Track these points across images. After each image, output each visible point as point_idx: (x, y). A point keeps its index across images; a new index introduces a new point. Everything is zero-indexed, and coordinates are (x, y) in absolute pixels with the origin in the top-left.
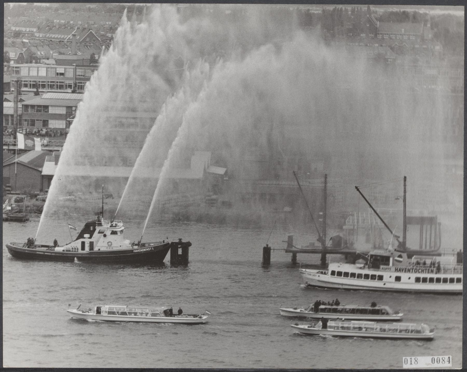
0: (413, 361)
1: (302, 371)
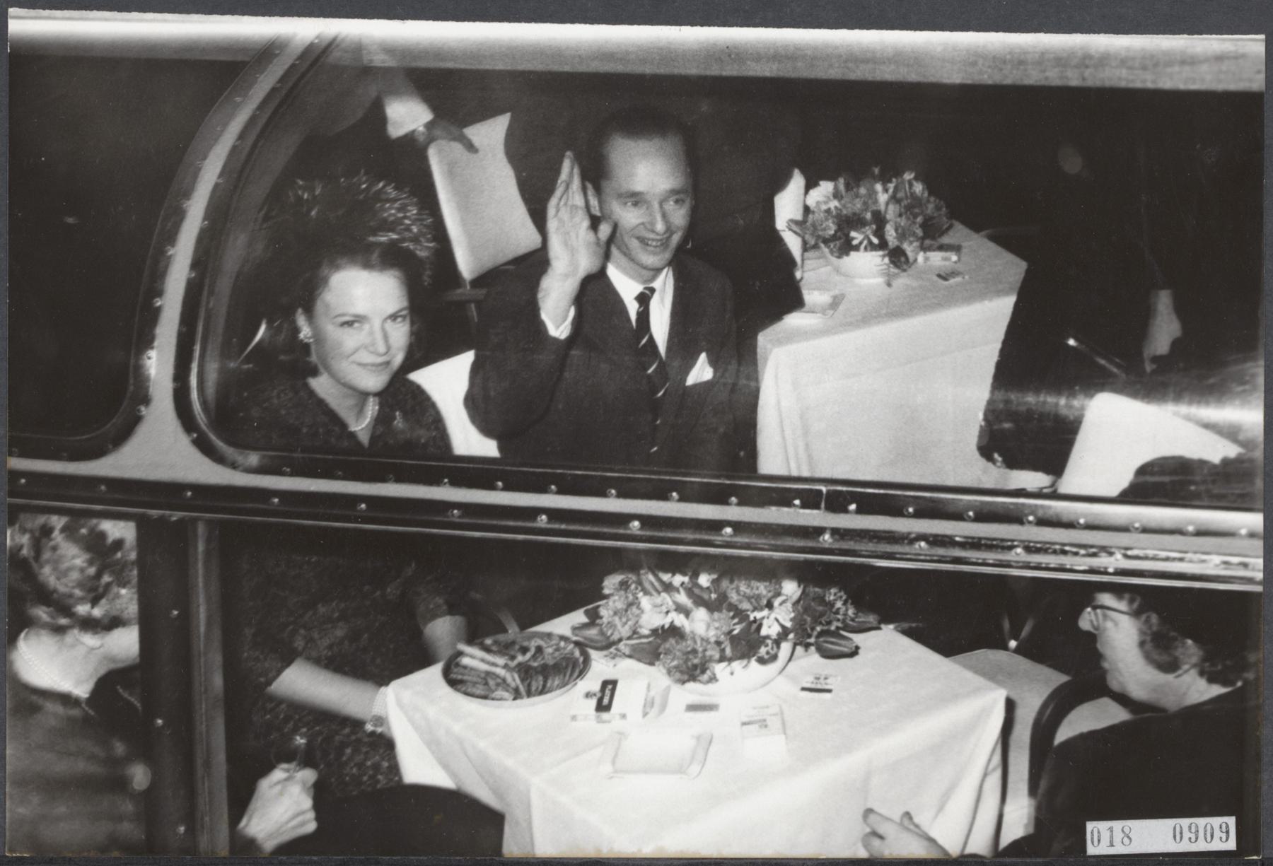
0: (1118, 836)
1: (830, 863)
